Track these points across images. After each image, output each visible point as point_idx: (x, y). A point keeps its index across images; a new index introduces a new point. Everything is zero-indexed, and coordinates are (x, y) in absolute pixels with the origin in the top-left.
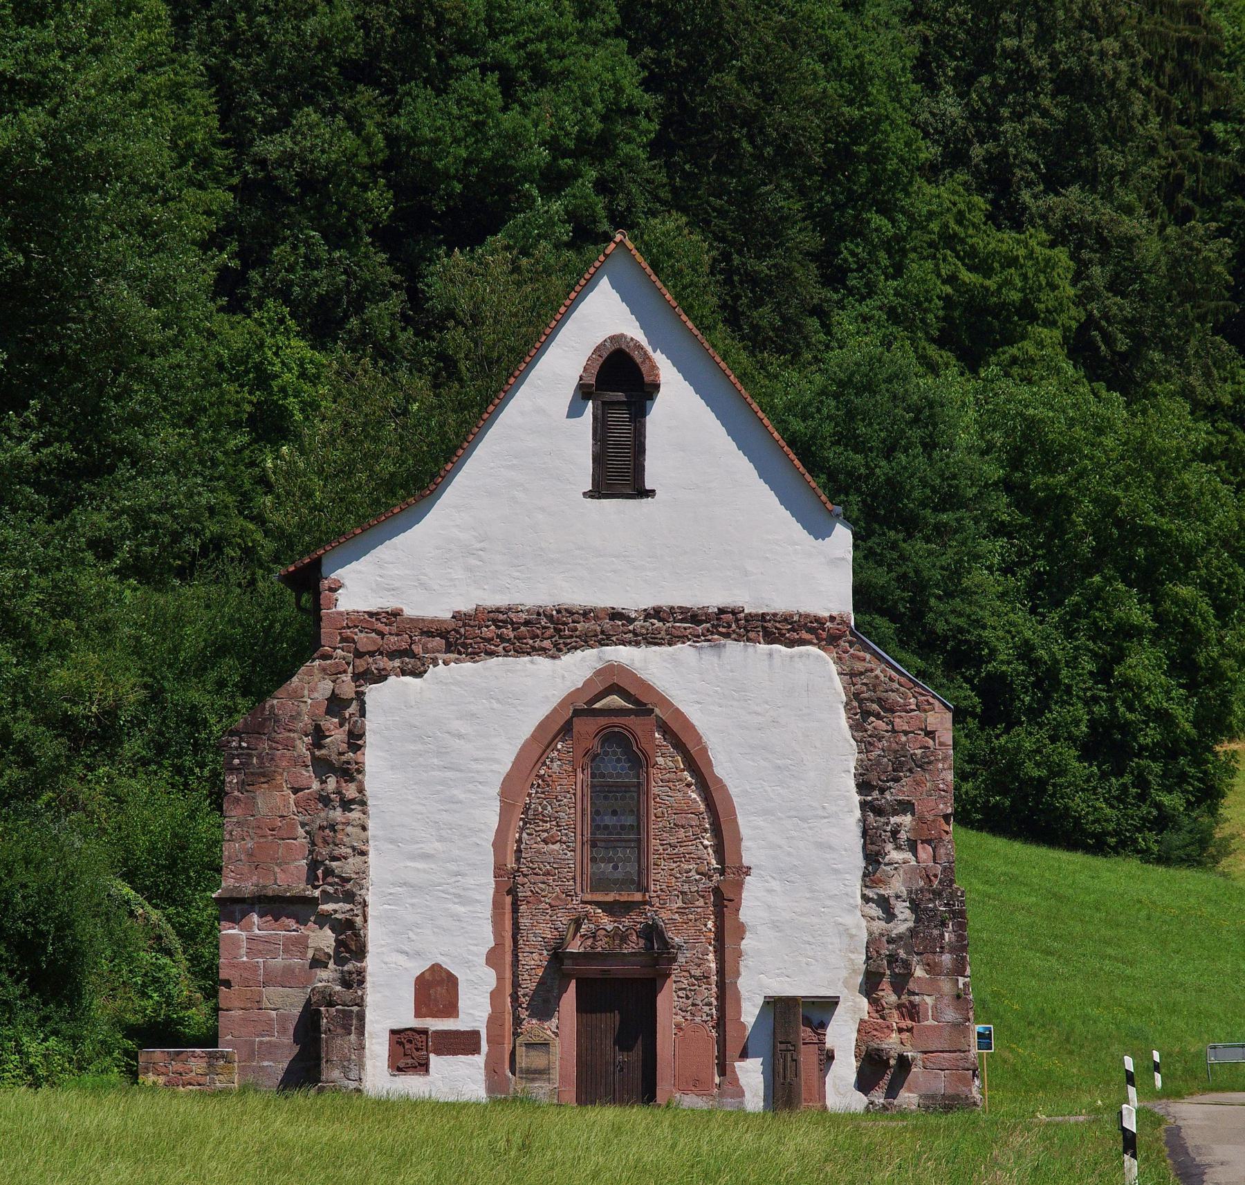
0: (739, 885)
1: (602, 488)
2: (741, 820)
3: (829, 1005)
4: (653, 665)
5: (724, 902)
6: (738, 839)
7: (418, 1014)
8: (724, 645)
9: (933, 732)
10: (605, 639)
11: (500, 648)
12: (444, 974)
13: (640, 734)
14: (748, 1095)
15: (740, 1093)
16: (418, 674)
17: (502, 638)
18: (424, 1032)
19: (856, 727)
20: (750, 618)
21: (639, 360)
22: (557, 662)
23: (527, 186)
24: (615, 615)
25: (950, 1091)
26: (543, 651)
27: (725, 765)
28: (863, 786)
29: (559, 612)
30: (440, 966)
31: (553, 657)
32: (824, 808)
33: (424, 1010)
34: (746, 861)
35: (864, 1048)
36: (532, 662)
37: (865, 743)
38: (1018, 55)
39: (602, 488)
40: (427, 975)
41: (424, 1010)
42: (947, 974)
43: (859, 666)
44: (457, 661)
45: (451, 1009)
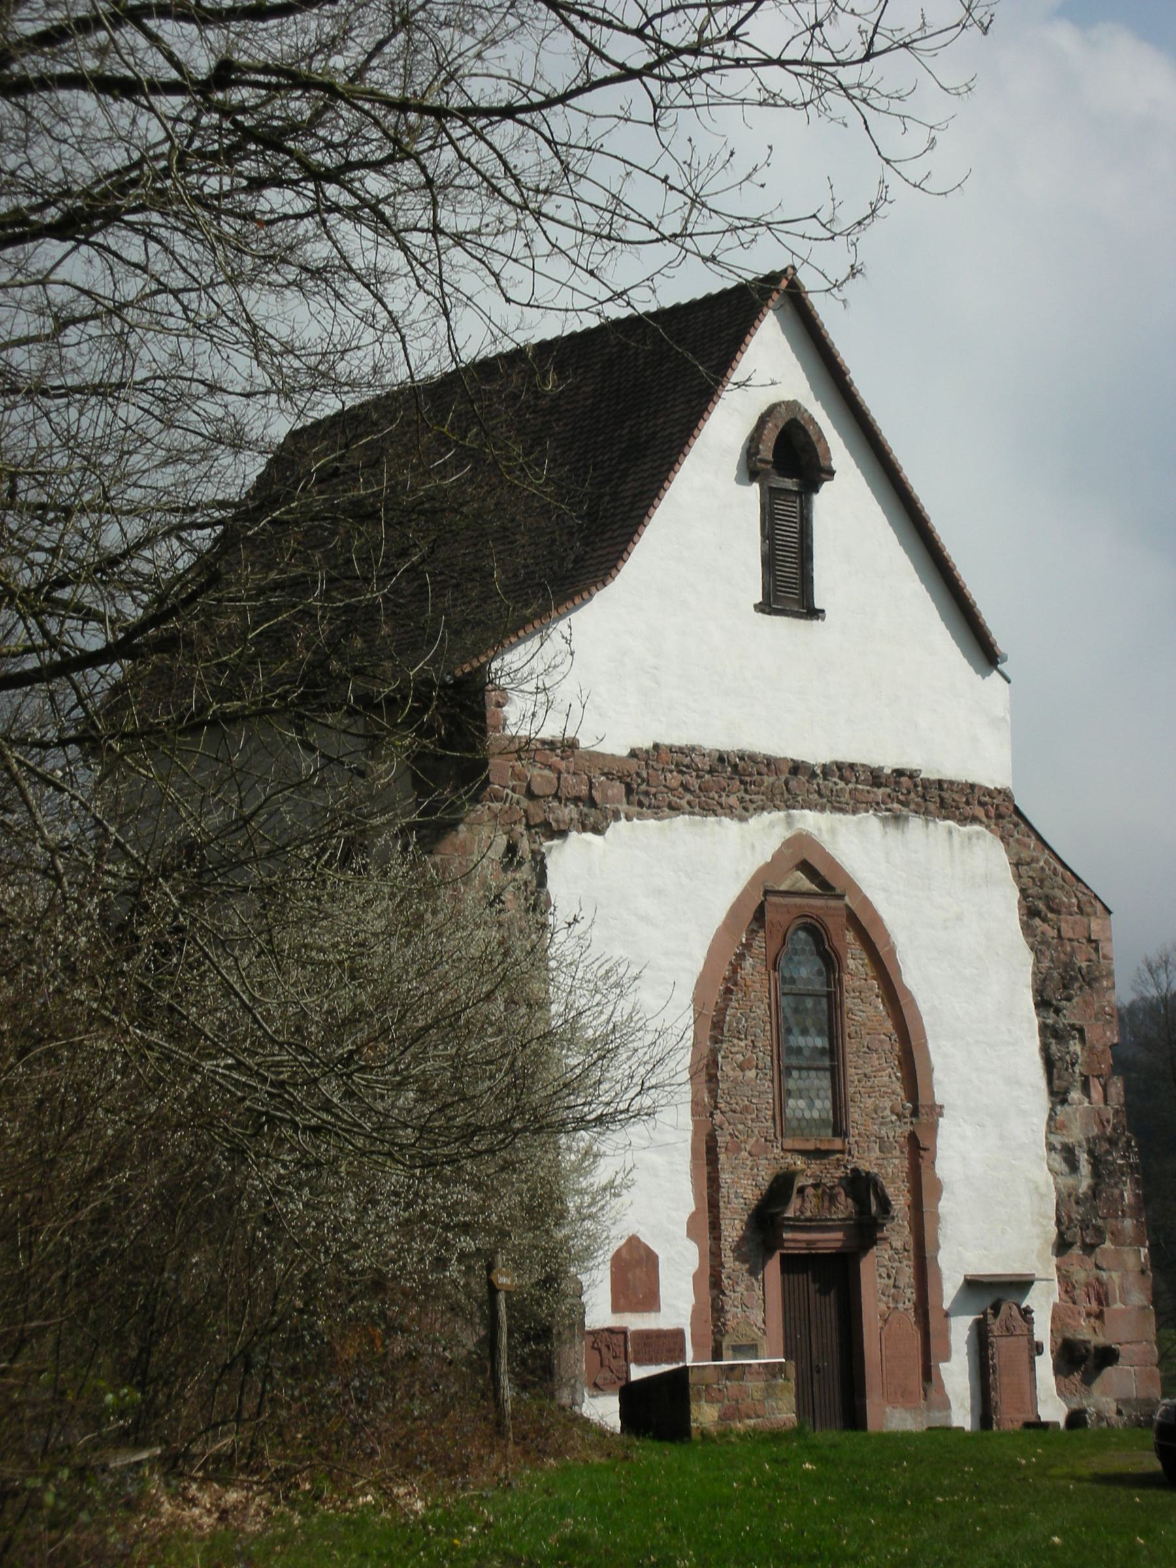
0: (933, 1128)
1: (767, 606)
2: (931, 1046)
3: (1023, 1285)
4: (859, 846)
5: (919, 1150)
6: (930, 1070)
7: (616, 1308)
8: (906, 818)
9: (1095, 941)
10: (788, 800)
11: (684, 803)
12: (642, 1252)
13: (833, 932)
14: (954, 1406)
15: (946, 1405)
16: (598, 830)
17: (685, 787)
18: (623, 1332)
19: (1027, 929)
20: (927, 784)
21: (814, 438)
22: (744, 825)
23: (411, 1094)
24: (797, 768)
25: (1143, 1395)
26: (729, 811)
27: (916, 974)
28: (1042, 1003)
29: (742, 758)
30: (638, 1239)
31: (742, 819)
32: (1009, 1031)
33: (622, 1302)
34: (939, 1100)
35: (1060, 1341)
36: (719, 823)
37: (1038, 946)
38: (124, 1072)
39: (767, 606)
40: (624, 1251)
41: (622, 1302)
42: (1130, 1245)
43: (1025, 855)
44: (641, 817)
45: (650, 1301)
